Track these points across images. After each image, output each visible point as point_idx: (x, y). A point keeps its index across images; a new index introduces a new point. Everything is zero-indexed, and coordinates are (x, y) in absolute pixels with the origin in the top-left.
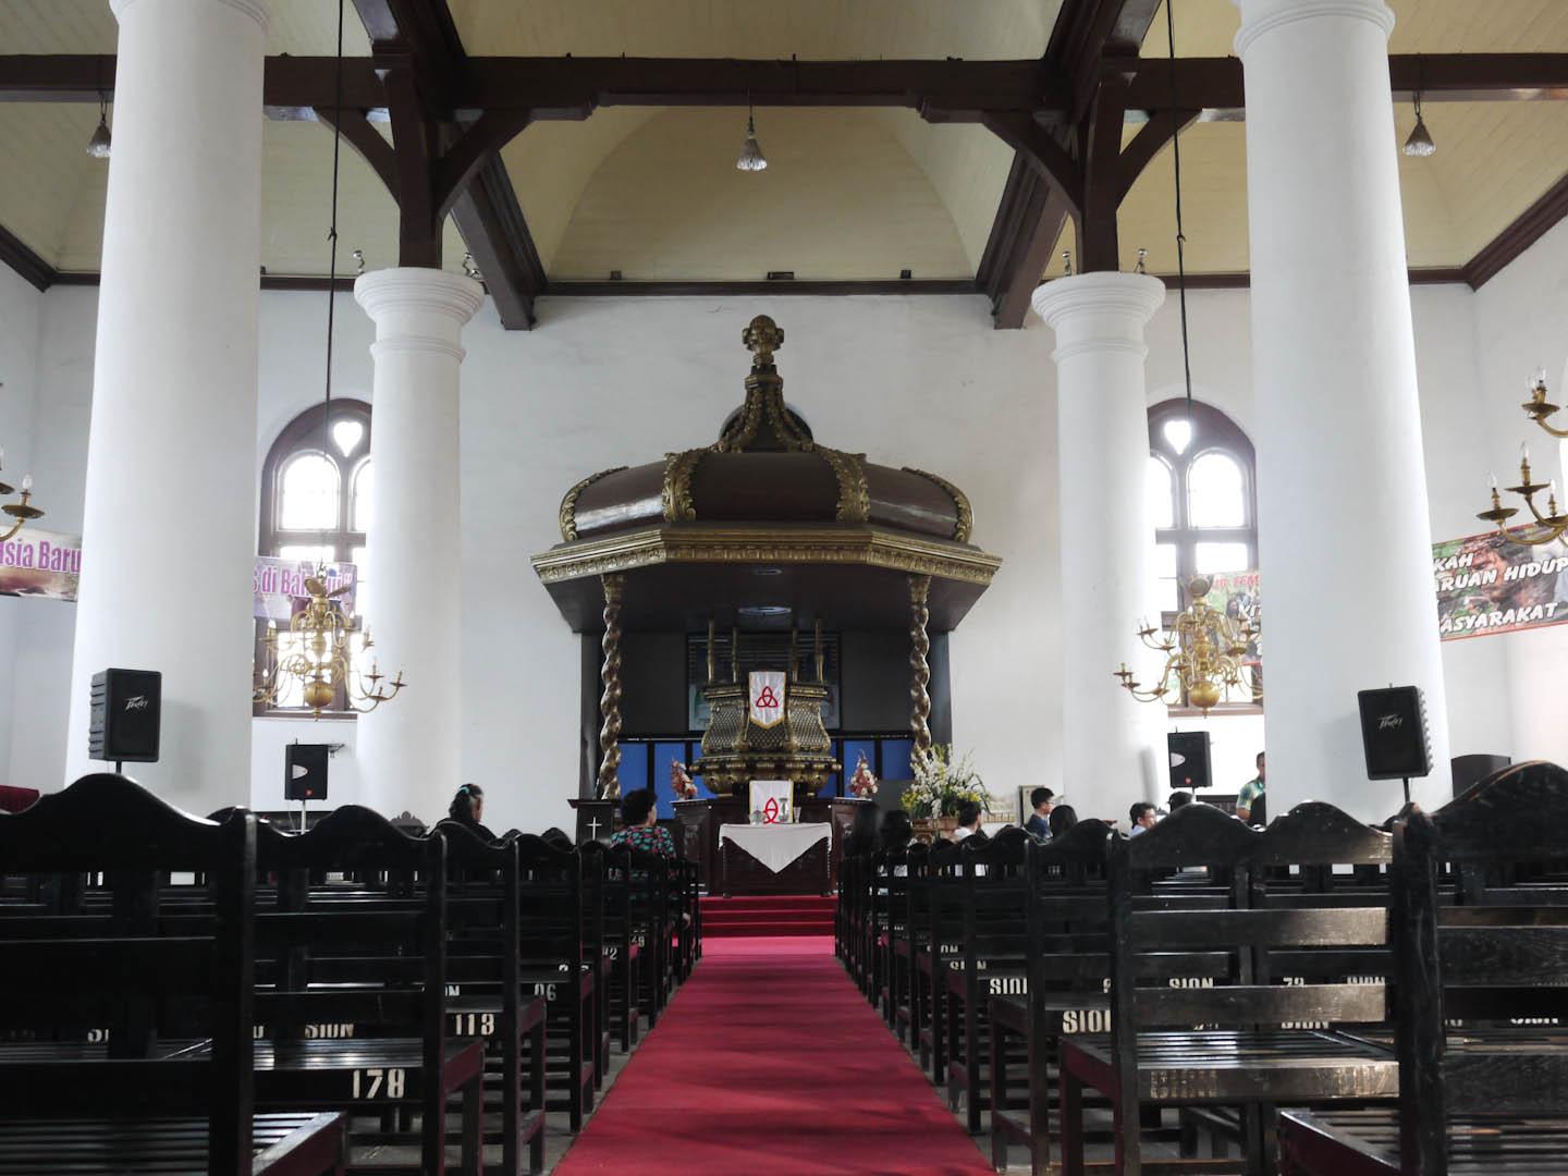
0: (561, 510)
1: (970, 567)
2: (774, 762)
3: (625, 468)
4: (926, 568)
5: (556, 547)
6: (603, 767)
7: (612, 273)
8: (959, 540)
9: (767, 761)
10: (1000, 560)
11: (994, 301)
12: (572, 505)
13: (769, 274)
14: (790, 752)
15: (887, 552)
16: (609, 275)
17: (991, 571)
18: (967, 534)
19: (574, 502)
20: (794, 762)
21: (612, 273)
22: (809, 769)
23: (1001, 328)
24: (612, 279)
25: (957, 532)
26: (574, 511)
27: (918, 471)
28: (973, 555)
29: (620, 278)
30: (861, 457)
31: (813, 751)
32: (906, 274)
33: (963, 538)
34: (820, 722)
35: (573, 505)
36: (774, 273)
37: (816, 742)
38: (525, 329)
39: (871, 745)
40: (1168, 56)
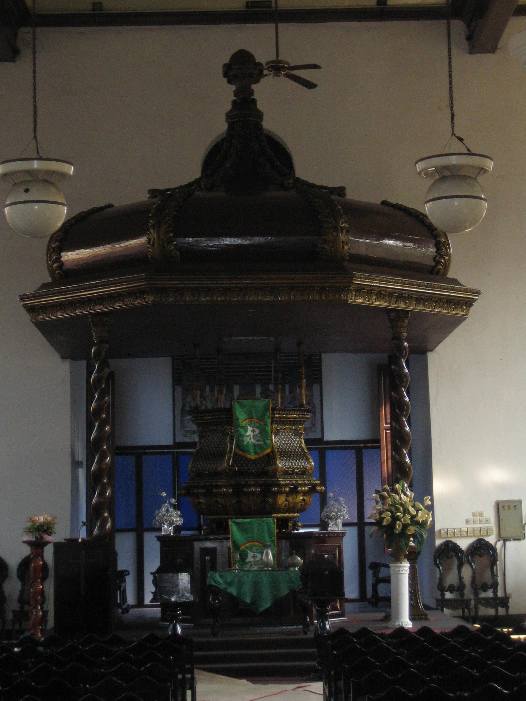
0: (48, 249)
1: (450, 302)
2: (260, 486)
3: (110, 206)
4: (406, 304)
5: (44, 286)
6: (94, 501)
7: (94, 4)
8: (438, 272)
9: (254, 485)
10: (478, 293)
11: (468, 26)
12: (57, 244)
13: (247, 3)
14: (275, 476)
15: (370, 292)
16: (90, 7)
17: (469, 303)
18: (446, 267)
19: (60, 241)
20: (279, 486)
21: (94, 4)
22: (294, 491)
23: (477, 52)
24: (93, 10)
25: (436, 265)
26: (61, 249)
27: (397, 204)
28: (453, 289)
29: (101, 9)
30: (341, 191)
31: (297, 473)
32: (97, 6)
33: (442, 271)
34: (303, 445)
35: (60, 244)
36: (252, 2)
37: (297, 464)
38: (7, 61)
39: (356, 521)
40: (279, 25)
